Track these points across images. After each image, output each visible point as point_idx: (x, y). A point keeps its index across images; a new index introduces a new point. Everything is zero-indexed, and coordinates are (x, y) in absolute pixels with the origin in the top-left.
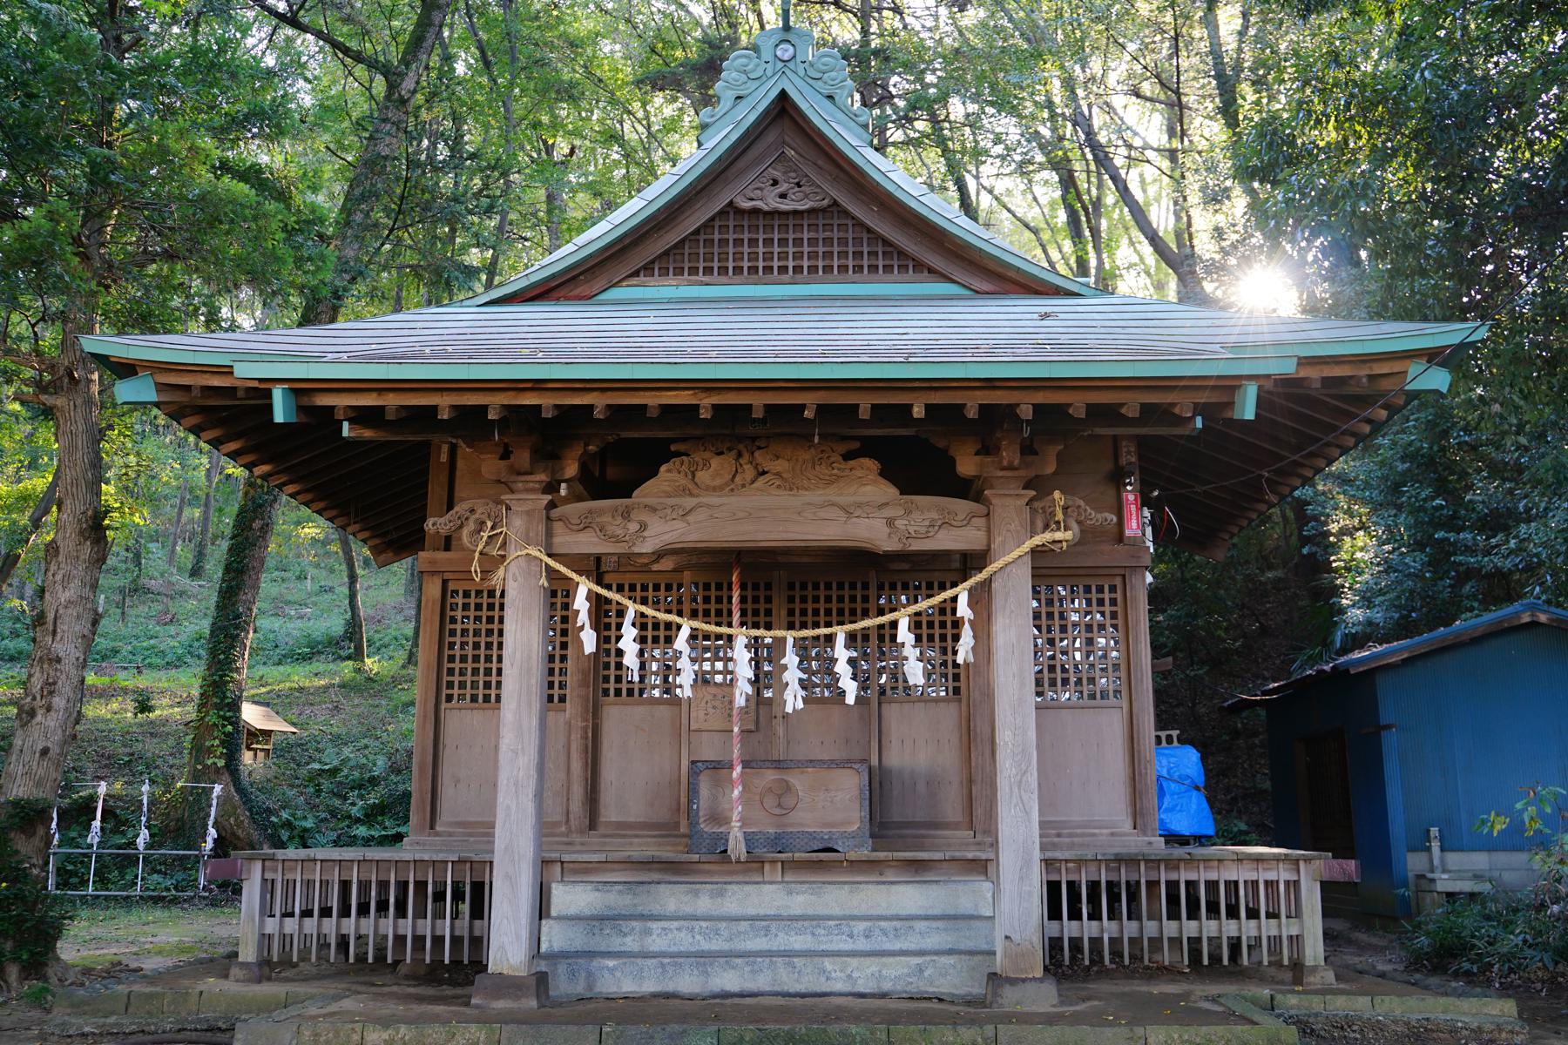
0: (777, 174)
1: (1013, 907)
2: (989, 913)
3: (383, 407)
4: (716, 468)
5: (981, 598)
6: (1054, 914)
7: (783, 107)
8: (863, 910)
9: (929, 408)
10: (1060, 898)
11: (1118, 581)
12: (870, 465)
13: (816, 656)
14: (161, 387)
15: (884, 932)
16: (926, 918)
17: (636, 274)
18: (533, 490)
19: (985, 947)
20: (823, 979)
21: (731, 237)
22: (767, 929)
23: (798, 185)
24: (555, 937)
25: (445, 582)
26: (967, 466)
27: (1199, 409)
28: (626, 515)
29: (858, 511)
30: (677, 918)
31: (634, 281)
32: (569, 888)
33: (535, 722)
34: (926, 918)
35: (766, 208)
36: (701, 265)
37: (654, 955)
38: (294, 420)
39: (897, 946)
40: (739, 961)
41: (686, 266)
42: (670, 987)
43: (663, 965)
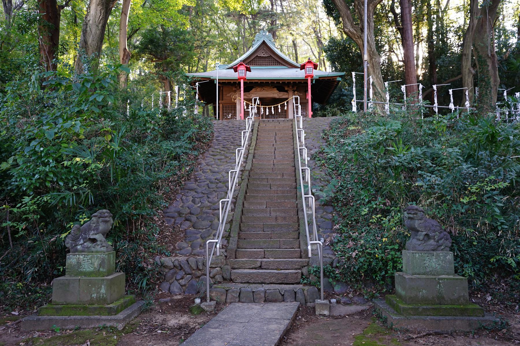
4: (259, 89)
5: (287, 103)
7: (264, 42)
13: (270, 109)
26: (286, 89)
29: (275, 94)
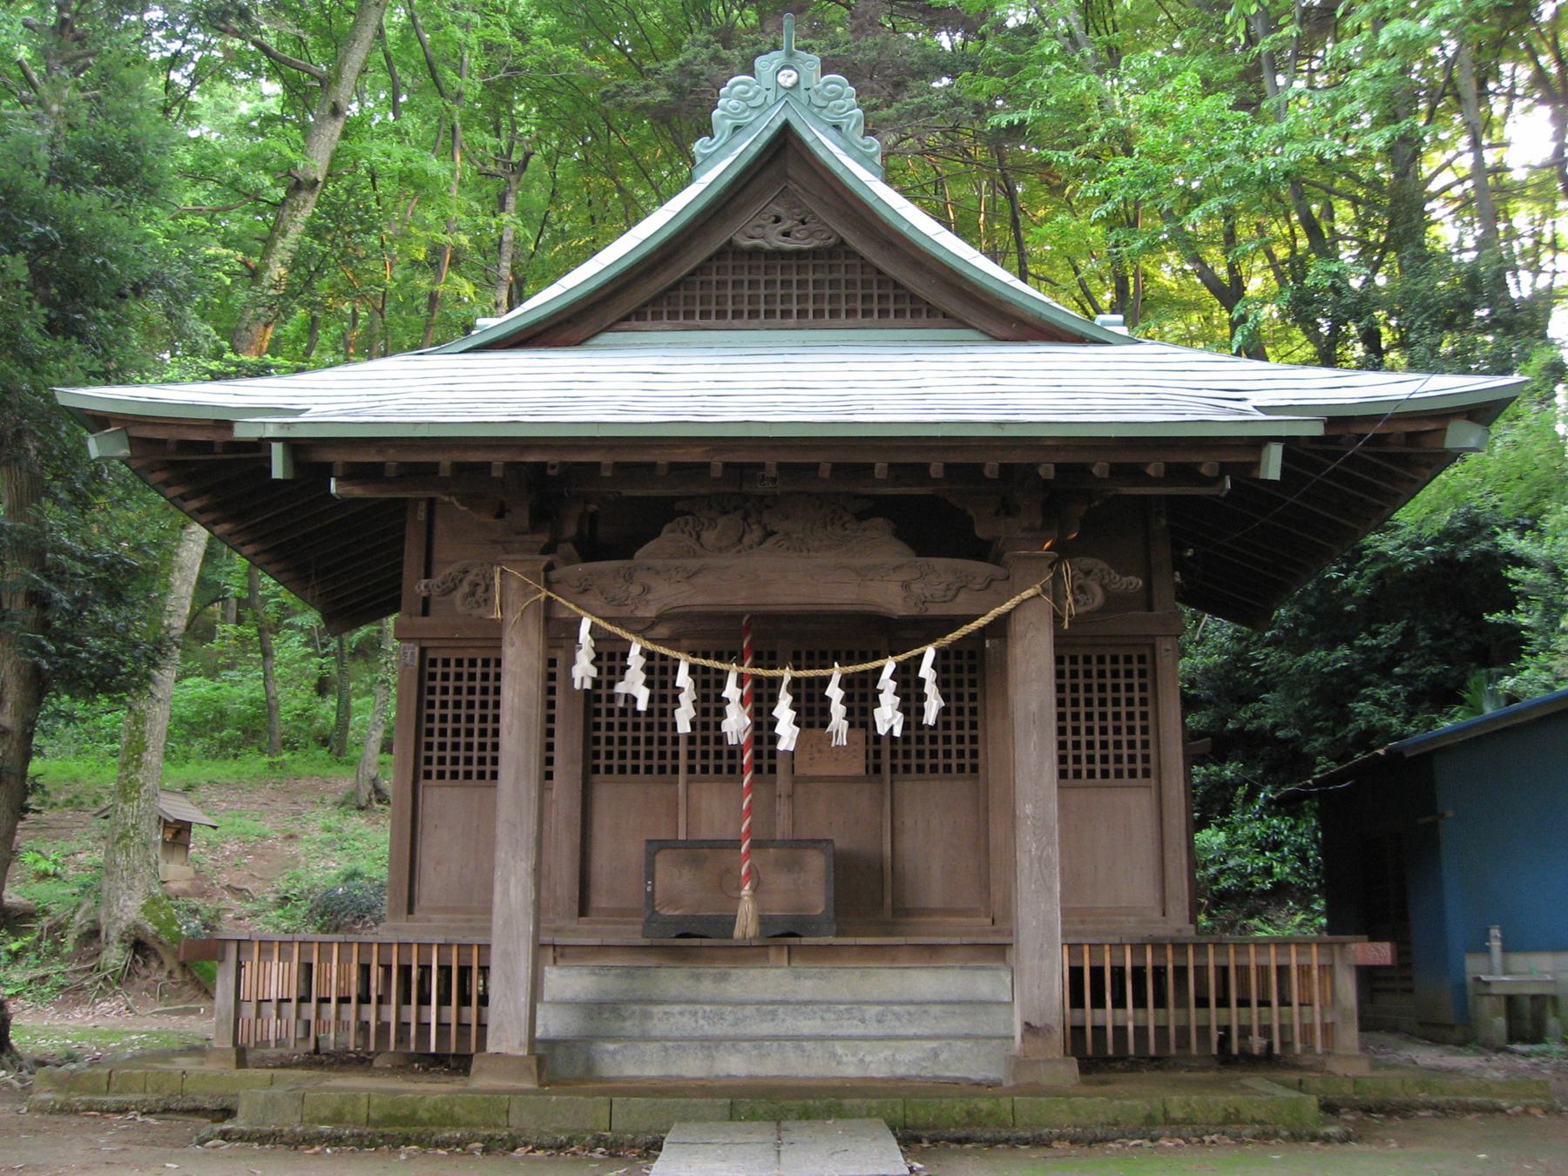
0: (778, 210)
1: (1036, 983)
2: (1007, 998)
3: (382, 464)
6: (1076, 1001)
8: (876, 995)
9: (947, 466)
10: (1083, 986)
11: (1147, 652)
12: (879, 527)
14: (134, 442)
15: (898, 1017)
16: (942, 1003)
17: (627, 318)
18: (530, 551)
19: (1004, 1032)
20: (834, 1064)
21: (730, 278)
22: (774, 1013)
23: (803, 222)
24: (551, 1024)
25: (423, 651)
27: (1225, 468)
28: (629, 577)
30: (679, 1003)
31: (625, 325)
32: (564, 972)
33: (534, 794)
34: (942, 1003)
35: (767, 246)
36: (698, 309)
37: (656, 1039)
38: (290, 477)
39: (912, 1031)
40: (746, 1044)
41: (682, 309)
42: (674, 1071)
43: (666, 1049)
